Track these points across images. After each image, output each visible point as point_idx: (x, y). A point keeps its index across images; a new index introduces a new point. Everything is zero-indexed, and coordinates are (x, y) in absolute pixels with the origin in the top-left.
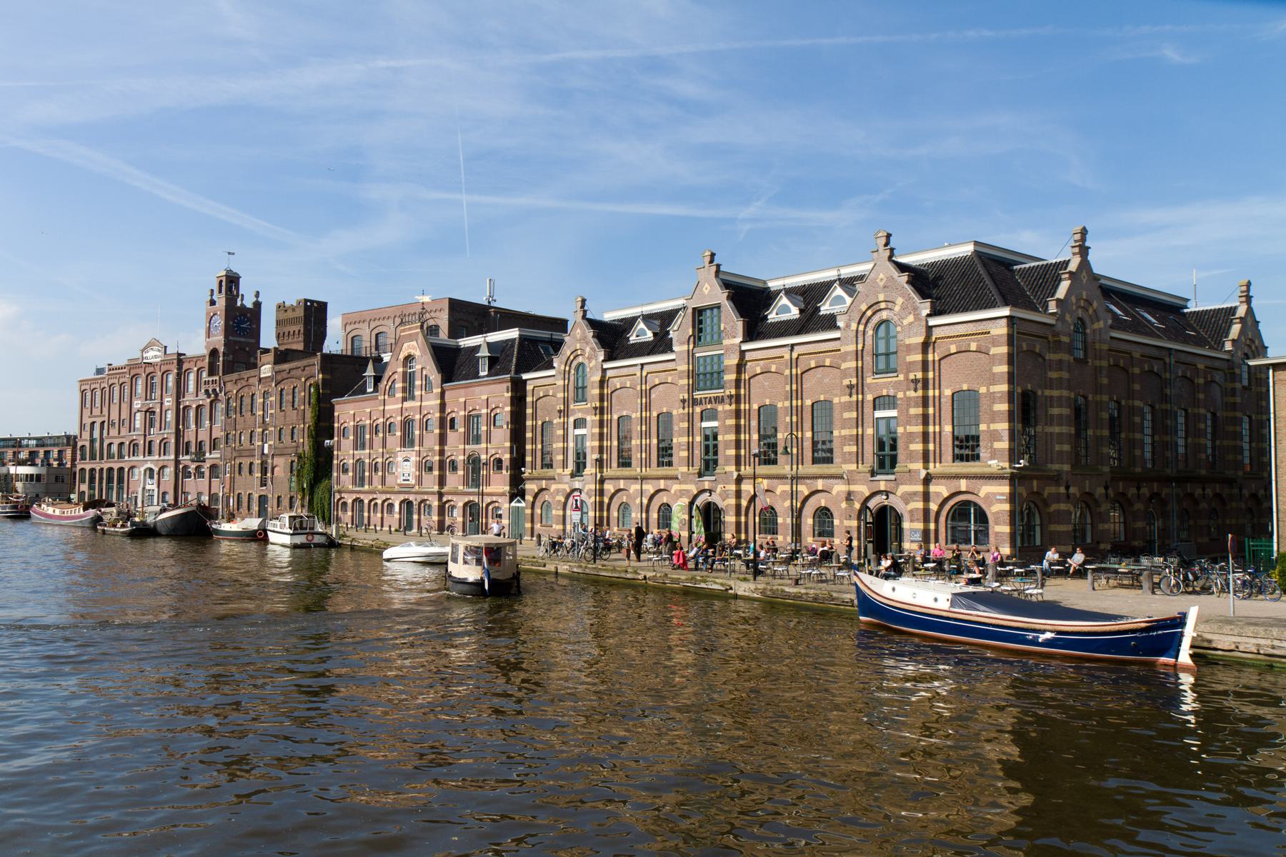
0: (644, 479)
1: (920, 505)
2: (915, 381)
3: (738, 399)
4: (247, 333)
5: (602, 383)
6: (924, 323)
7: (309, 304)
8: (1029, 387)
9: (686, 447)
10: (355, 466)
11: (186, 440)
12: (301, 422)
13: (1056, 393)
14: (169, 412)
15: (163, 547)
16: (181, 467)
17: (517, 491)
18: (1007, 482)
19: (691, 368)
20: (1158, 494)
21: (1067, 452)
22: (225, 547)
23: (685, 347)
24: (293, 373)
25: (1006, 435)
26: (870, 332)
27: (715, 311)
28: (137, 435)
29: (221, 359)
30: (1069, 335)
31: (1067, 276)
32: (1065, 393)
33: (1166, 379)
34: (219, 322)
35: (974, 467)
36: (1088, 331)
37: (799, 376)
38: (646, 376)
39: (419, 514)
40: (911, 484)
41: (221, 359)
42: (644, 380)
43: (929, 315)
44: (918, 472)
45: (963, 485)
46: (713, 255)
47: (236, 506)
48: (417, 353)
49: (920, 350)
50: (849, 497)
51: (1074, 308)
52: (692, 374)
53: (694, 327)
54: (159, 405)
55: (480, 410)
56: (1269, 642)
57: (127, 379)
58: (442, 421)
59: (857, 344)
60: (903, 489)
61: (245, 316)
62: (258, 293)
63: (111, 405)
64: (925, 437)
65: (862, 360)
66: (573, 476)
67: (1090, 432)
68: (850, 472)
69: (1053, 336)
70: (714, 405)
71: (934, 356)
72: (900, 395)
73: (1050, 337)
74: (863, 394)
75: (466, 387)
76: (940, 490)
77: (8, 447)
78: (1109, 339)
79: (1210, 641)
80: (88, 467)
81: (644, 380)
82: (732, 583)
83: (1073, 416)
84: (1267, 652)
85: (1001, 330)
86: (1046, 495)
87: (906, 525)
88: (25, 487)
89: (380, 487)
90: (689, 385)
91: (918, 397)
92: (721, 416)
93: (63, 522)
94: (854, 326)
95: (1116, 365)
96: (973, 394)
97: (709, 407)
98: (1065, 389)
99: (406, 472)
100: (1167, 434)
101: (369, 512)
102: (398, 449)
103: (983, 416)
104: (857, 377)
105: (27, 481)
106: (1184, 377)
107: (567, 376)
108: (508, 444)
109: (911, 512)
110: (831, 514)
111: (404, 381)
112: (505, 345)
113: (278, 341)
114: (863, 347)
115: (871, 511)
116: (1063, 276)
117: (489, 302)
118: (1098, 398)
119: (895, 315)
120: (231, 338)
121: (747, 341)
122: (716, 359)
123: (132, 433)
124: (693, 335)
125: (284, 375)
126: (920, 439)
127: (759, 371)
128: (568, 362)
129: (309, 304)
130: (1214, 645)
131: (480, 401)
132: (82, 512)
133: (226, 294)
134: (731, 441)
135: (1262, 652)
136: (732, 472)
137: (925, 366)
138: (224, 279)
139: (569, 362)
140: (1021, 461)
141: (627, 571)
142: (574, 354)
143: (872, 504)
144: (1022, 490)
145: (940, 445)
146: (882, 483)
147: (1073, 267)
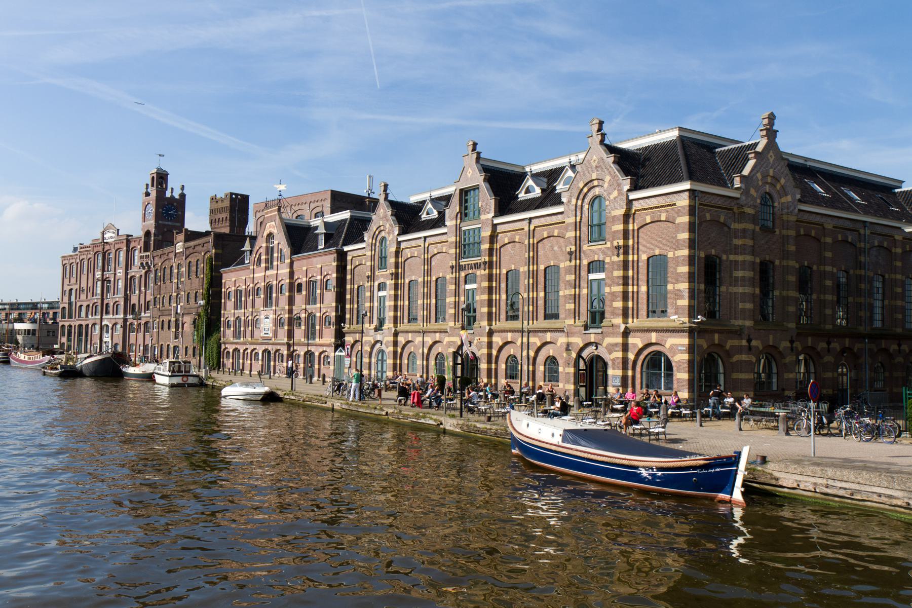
0: (424, 332)
1: (619, 355)
2: (618, 248)
3: (490, 265)
4: (171, 219)
5: (398, 253)
6: (625, 197)
7: (234, 196)
8: (713, 252)
9: (453, 306)
10: (235, 322)
11: (132, 303)
12: (201, 287)
13: (740, 258)
14: (120, 281)
15: (87, 384)
16: (128, 323)
17: (340, 344)
18: (687, 334)
19: (458, 240)
20: (850, 349)
21: (749, 310)
22: (134, 384)
23: (454, 222)
24: (197, 248)
25: (686, 294)
26: (586, 206)
27: (477, 190)
28: (97, 299)
29: (152, 238)
30: (755, 208)
31: (753, 155)
32: (749, 258)
33: (860, 248)
34: (152, 209)
35: (662, 321)
36: (776, 204)
37: (535, 245)
38: (428, 247)
39: (275, 361)
40: (613, 337)
41: (152, 238)
42: (426, 250)
43: (629, 191)
44: (618, 325)
45: (654, 337)
46: (475, 145)
47: (159, 355)
48: (275, 231)
49: (622, 221)
50: (568, 347)
51: (760, 183)
52: (458, 245)
53: (460, 205)
54: (113, 275)
55: (316, 276)
56: (824, 482)
57: (91, 256)
58: (291, 285)
59: (576, 216)
60: (608, 340)
61: (172, 205)
62: (183, 186)
63: (82, 276)
64: (625, 296)
65: (580, 230)
66: (376, 330)
67: (776, 293)
68: (569, 326)
69: (739, 208)
70: (474, 270)
71: (634, 226)
72: (607, 260)
73: (735, 209)
74: (580, 259)
75: (308, 257)
76: (636, 341)
77: (28, 309)
78: (797, 210)
79: (777, 479)
80: (67, 324)
81: (426, 250)
82: (442, 419)
83: (757, 278)
84: (822, 491)
85: (683, 202)
86: (728, 347)
87: (610, 372)
88: (23, 340)
89: (250, 339)
90: (456, 253)
91: (619, 261)
92: (478, 279)
93: (29, 366)
94: (574, 201)
95: (807, 235)
96: (663, 258)
97: (470, 271)
98: (749, 254)
99: (266, 327)
100: (861, 296)
101: (319, 364)
102: (262, 309)
103: (670, 277)
104: (576, 245)
105: (25, 334)
106: (881, 246)
107: (373, 248)
108: (334, 304)
109: (613, 360)
110: (557, 362)
111: (267, 254)
112: (339, 224)
113: (211, 225)
114: (581, 219)
115: (584, 360)
116: (750, 156)
117: (369, 194)
118: (785, 263)
119: (605, 191)
120: (160, 222)
121: (498, 216)
122: (476, 231)
123: (115, 296)
124: (460, 212)
125: (191, 250)
126: (620, 298)
127: (506, 242)
128: (374, 237)
129: (234, 196)
130: (780, 483)
131: (316, 269)
132: (41, 358)
133: (157, 187)
134: (485, 300)
135: (818, 490)
136: (485, 327)
137: (626, 234)
138: (155, 175)
139: (375, 236)
140: (699, 317)
141: (376, 408)
142: (379, 230)
143: (585, 354)
144: (703, 343)
145: (638, 303)
146: (592, 336)
147: (759, 148)
